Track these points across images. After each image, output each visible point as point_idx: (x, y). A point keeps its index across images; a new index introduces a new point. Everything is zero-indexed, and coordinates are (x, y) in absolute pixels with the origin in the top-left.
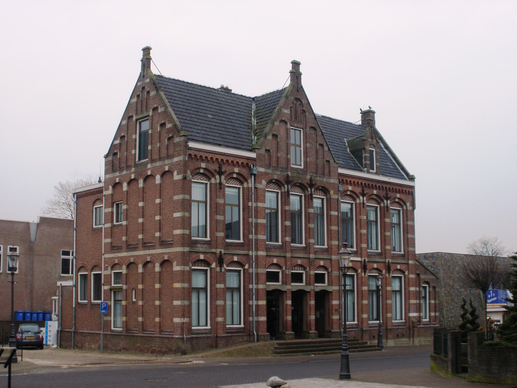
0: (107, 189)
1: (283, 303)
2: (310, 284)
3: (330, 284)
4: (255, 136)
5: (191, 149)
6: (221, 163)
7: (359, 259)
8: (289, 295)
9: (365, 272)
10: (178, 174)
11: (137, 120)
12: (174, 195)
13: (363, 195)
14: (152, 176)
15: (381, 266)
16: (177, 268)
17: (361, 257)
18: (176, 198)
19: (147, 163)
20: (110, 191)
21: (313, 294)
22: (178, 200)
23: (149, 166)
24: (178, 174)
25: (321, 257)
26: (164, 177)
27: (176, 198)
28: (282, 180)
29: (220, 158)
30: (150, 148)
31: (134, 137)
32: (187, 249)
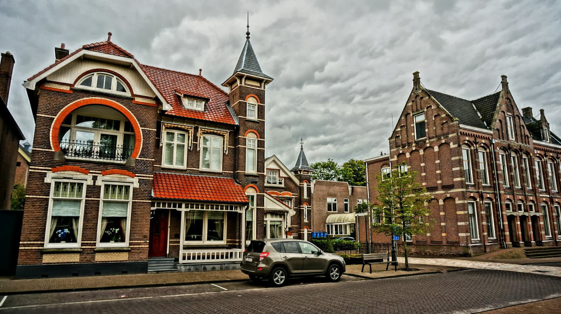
0: (392, 157)
1: (515, 224)
2: (516, 211)
3: (537, 211)
4: (453, 121)
5: (461, 128)
6: (476, 137)
7: (548, 196)
8: (518, 218)
9: (482, 201)
10: (454, 144)
11: (413, 115)
12: (452, 157)
13: (546, 156)
14: (431, 147)
15: (476, 195)
16: (458, 202)
17: (549, 195)
18: (453, 159)
19: (426, 140)
20: (395, 158)
21: (530, 217)
22: (456, 160)
23: (427, 141)
24: (454, 144)
25: (488, 192)
26: (441, 147)
27: (453, 159)
28: (507, 147)
29: (475, 134)
30: (427, 130)
31: (412, 125)
32: (464, 190)
